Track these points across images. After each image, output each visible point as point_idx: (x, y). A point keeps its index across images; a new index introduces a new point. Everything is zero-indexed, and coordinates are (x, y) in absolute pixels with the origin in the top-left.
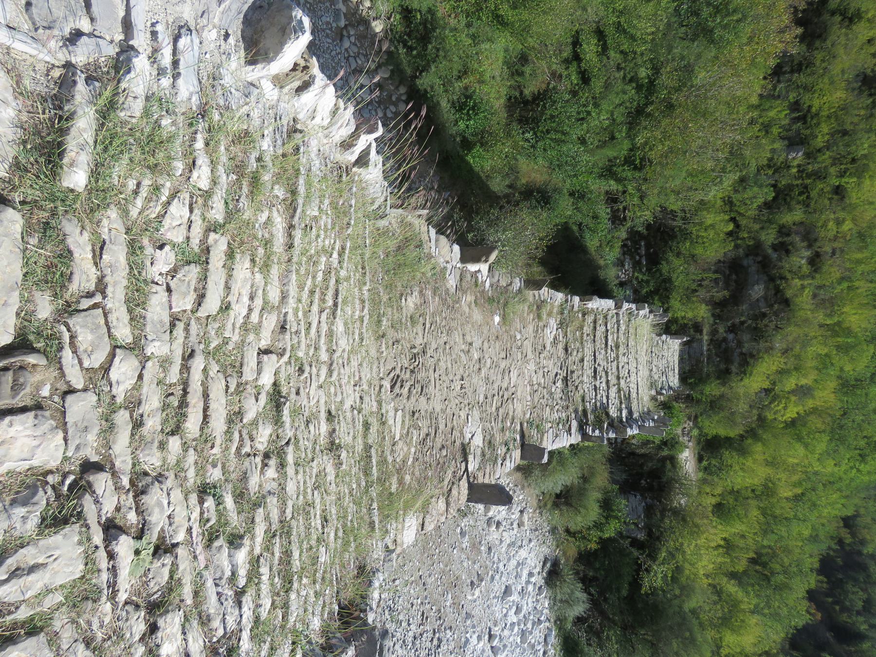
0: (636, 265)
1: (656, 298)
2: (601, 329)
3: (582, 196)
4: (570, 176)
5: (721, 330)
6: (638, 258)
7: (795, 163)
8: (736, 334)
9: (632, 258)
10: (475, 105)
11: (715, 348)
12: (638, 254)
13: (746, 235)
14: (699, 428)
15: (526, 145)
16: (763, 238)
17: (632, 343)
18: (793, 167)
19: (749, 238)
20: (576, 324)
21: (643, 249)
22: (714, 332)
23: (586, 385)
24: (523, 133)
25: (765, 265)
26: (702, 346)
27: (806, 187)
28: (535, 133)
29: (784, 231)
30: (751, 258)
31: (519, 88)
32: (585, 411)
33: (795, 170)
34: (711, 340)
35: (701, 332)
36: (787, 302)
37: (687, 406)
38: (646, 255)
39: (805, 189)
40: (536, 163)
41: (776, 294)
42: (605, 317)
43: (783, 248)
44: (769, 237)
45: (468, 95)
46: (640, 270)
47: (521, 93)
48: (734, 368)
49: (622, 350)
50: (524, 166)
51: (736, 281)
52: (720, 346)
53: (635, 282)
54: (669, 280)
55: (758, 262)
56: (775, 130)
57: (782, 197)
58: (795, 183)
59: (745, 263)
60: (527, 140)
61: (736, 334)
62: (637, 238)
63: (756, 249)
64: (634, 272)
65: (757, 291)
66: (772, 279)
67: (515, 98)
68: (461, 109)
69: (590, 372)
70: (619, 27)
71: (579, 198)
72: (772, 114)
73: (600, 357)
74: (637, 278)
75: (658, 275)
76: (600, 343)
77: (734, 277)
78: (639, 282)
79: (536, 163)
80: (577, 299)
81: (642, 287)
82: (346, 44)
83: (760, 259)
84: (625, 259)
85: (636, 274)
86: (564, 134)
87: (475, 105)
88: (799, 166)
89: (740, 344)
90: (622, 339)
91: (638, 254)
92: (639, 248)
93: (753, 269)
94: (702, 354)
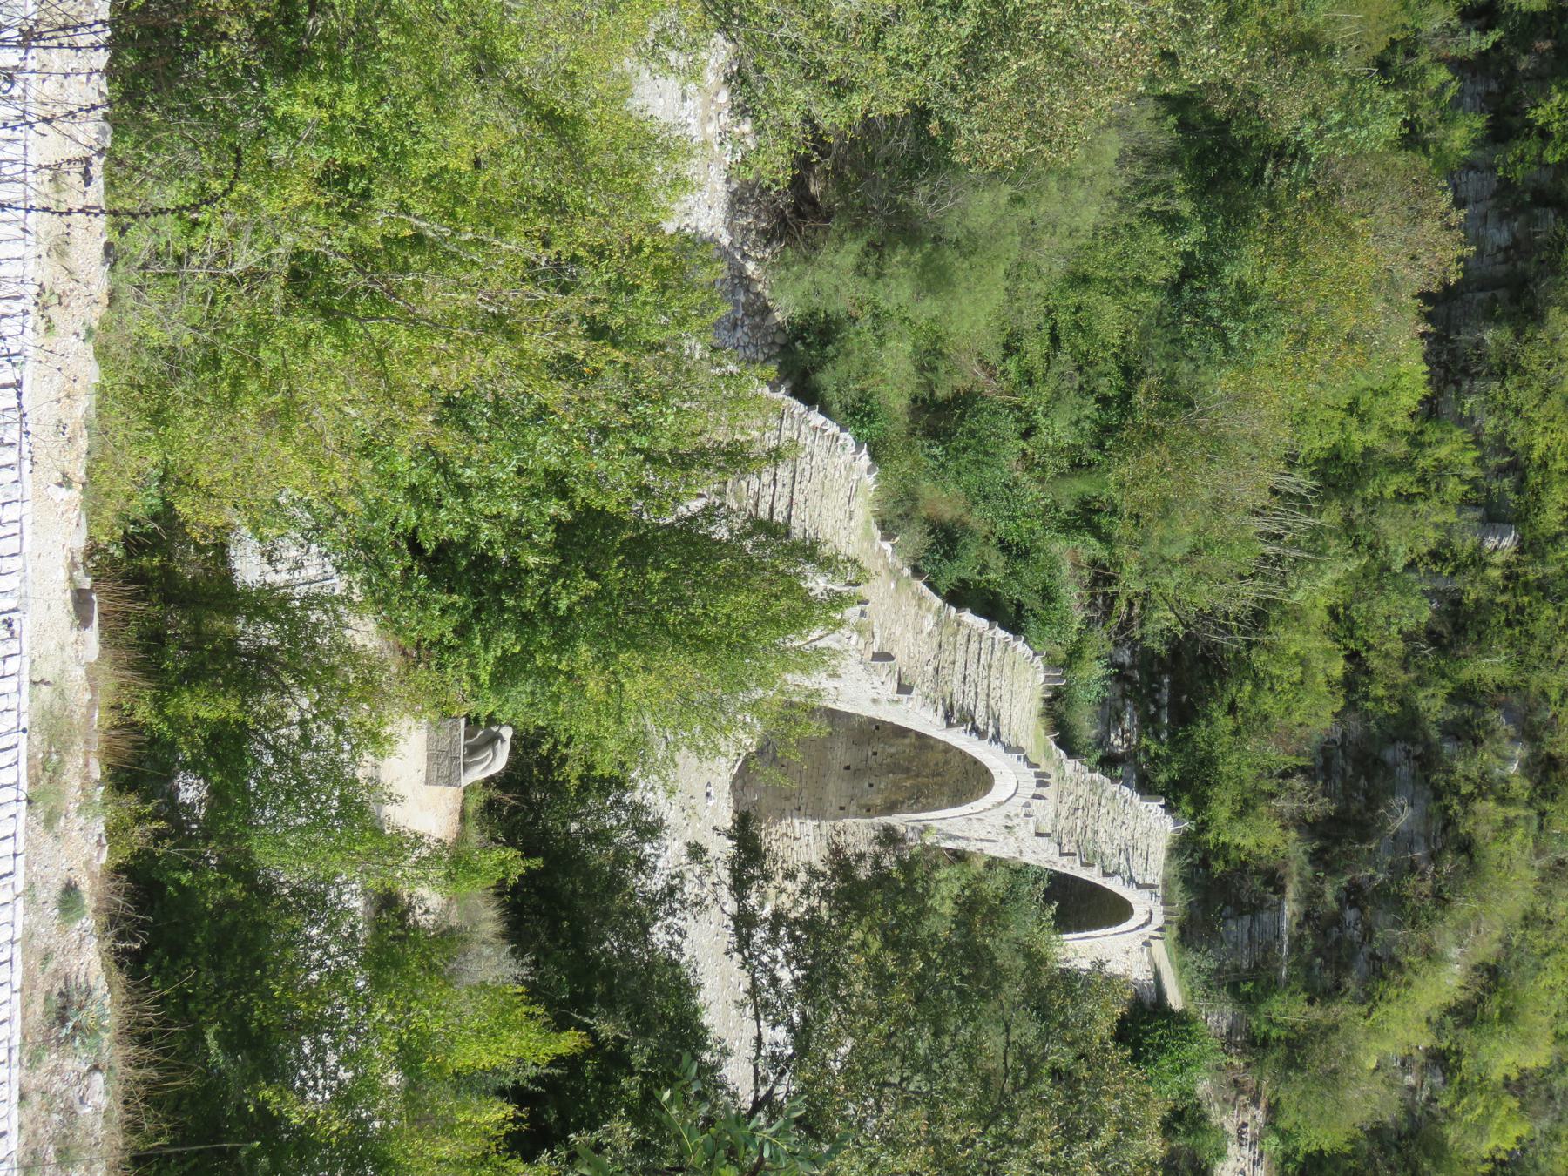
0: (1148, 722)
1: (1186, 798)
2: (974, 646)
3: (1024, 554)
4: (1003, 517)
5: (1330, 893)
6: (1152, 709)
7: (1498, 558)
8: (1362, 910)
9: (1140, 706)
10: (872, 410)
11: (1315, 937)
12: (1155, 702)
13: (1381, 692)
14: (1284, 1135)
15: (931, 463)
16: (1423, 704)
17: (1007, 670)
18: (1495, 566)
19: (1391, 698)
20: (950, 630)
21: (1165, 691)
22: (1311, 897)
23: (956, 685)
24: (930, 446)
25: (1427, 762)
26: (1279, 919)
27: (1520, 609)
28: (945, 449)
29: (1464, 694)
30: (1400, 745)
31: (930, 386)
32: (951, 706)
33: (1495, 574)
34: (1307, 916)
35: (1280, 890)
36: (1466, 847)
37: (1248, 1065)
38: (1169, 705)
39: (1518, 618)
40: (945, 490)
41: (1444, 829)
42: (980, 635)
43: (1465, 733)
44: (1433, 704)
45: (865, 397)
46: (1157, 735)
47: (932, 393)
48: (1351, 983)
49: (994, 672)
50: (927, 492)
51: (1366, 793)
52: (1325, 934)
53: (1143, 759)
54: (1209, 761)
55: (1415, 758)
56: (1454, 488)
57: (1456, 627)
58: (1500, 599)
59: (1389, 754)
60: (935, 457)
61: (1362, 910)
62: (1155, 668)
63: (1407, 724)
64: (1139, 737)
65: (1402, 815)
66: (1438, 795)
67: (924, 401)
68: (853, 414)
69: (961, 677)
70: (1077, 326)
71: (1018, 556)
72: (1443, 452)
73: (972, 669)
74: (1147, 750)
75: (1188, 749)
76: (972, 658)
77: (1362, 782)
78: (1151, 760)
79: (945, 490)
80: (953, 610)
81: (1157, 771)
82: (739, 333)
83: (1419, 750)
84: (1124, 707)
85: (1144, 741)
86: (987, 454)
87: (872, 410)
88: (1507, 565)
89: (1368, 934)
90: (995, 663)
91: (1155, 702)
92: (1158, 690)
93: (1404, 770)
94: (1278, 937)
